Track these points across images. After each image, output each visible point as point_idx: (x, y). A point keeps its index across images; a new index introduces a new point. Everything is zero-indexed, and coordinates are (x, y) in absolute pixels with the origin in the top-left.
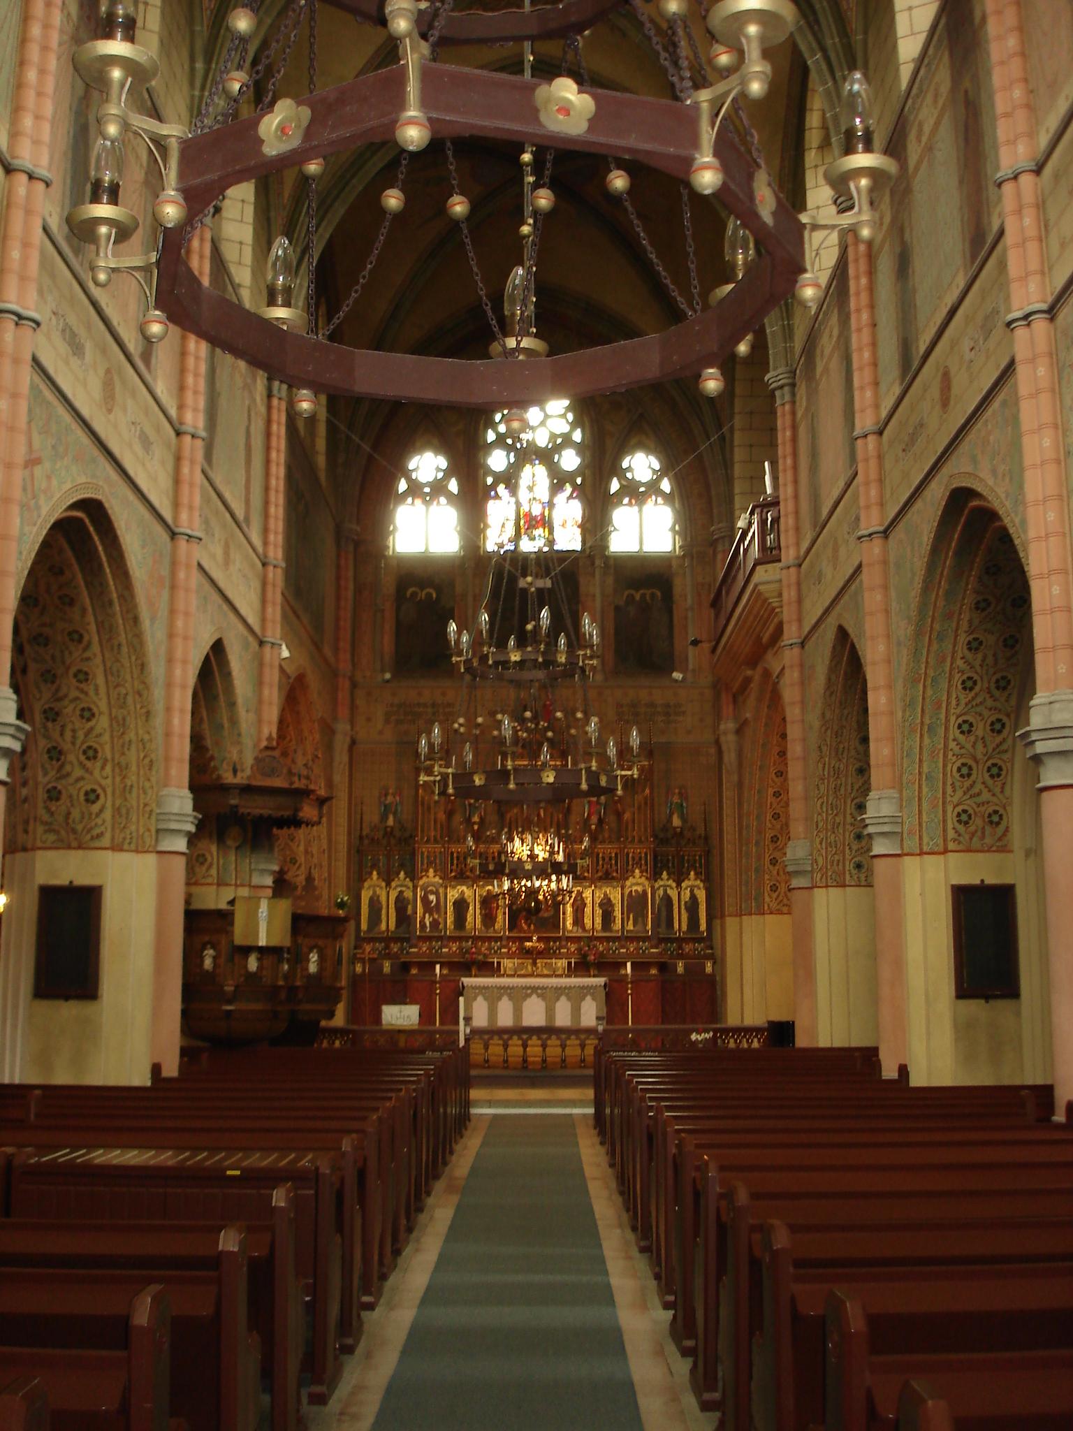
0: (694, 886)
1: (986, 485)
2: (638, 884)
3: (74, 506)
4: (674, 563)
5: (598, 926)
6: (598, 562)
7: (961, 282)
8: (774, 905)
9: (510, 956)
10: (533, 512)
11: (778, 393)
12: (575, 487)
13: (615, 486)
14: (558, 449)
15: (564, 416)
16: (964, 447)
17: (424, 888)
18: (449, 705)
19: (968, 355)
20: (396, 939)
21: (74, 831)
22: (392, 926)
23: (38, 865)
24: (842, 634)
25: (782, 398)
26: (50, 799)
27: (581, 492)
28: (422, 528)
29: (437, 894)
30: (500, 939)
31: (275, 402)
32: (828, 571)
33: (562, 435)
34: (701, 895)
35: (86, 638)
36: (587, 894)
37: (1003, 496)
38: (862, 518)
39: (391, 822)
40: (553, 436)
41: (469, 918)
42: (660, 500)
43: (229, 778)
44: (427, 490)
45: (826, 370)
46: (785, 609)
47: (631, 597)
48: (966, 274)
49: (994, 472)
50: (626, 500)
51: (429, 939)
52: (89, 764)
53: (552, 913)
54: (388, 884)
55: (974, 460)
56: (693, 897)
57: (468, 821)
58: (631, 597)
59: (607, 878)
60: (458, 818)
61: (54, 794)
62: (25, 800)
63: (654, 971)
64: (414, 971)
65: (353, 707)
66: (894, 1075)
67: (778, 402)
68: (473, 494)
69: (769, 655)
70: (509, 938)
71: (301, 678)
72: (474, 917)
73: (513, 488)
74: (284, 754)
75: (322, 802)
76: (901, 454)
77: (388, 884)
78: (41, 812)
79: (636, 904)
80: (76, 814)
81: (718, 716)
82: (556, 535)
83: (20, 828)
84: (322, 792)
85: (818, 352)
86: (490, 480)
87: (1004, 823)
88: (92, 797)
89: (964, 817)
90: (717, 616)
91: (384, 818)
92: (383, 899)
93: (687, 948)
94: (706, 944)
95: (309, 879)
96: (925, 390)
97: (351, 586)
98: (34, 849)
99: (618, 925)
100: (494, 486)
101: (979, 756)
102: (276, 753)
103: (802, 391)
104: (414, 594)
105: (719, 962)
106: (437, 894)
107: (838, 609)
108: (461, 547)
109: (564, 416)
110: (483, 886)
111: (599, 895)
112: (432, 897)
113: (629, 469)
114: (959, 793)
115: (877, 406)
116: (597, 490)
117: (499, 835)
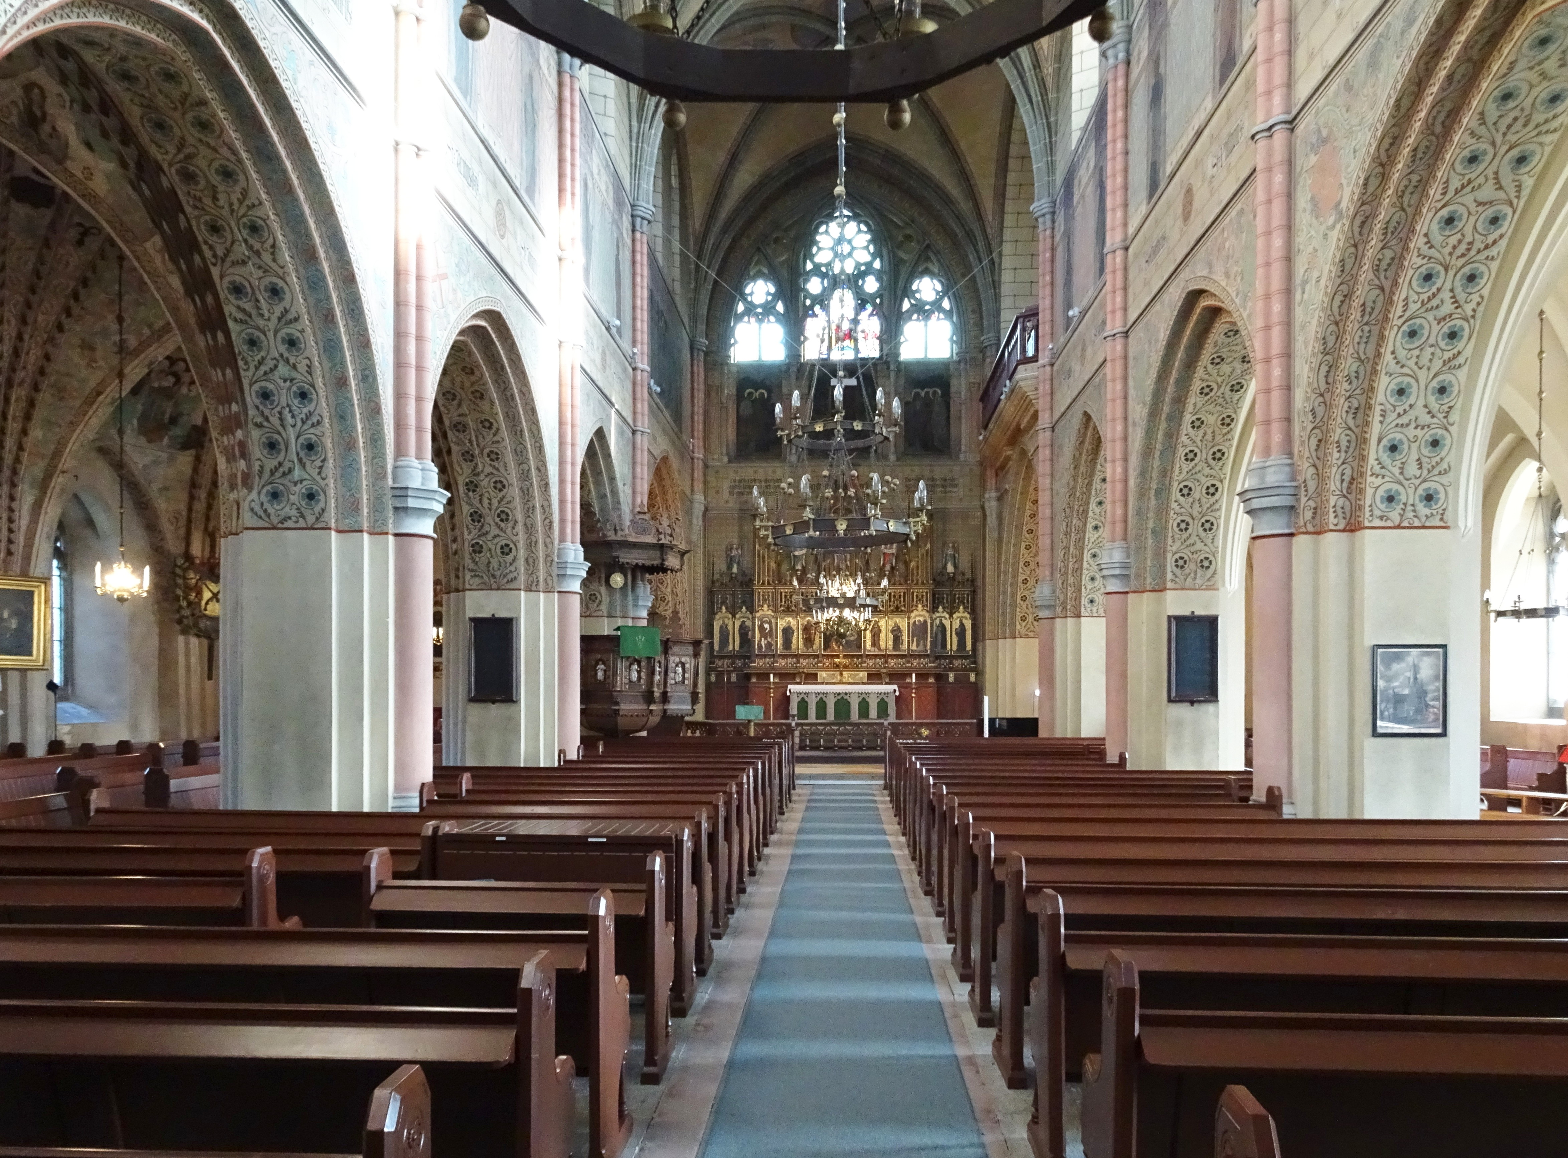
0: (962, 617)
1: (1219, 285)
3: (477, 316)
4: (952, 367)
5: (890, 647)
6: (892, 367)
7: (1209, 104)
8: (1023, 631)
9: (826, 669)
10: (840, 331)
11: (1040, 220)
12: (874, 305)
13: (906, 305)
14: (862, 275)
15: (867, 248)
16: (1202, 252)
17: (761, 619)
19: (1210, 171)
20: (740, 657)
21: (494, 576)
22: (737, 648)
23: (468, 602)
24: (1087, 417)
25: (1044, 224)
26: (474, 551)
27: (879, 311)
28: (756, 342)
29: (770, 623)
30: (817, 656)
31: (638, 235)
32: (1077, 367)
33: (866, 264)
34: (968, 624)
35: (495, 425)
36: (882, 623)
37: (1234, 295)
38: (1109, 322)
39: (735, 569)
40: (858, 265)
41: (794, 641)
42: (942, 316)
43: (611, 536)
44: (759, 310)
45: (1083, 196)
46: (1041, 401)
47: (917, 394)
48: (1214, 97)
49: (1227, 275)
50: (915, 316)
51: (765, 656)
52: (502, 525)
54: (734, 616)
55: (1210, 266)
56: (962, 625)
57: (793, 570)
58: (917, 394)
59: (897, 610)
60: (785, 567)
61: (477, 548)
62: (456, 553)
63: (931, 680)
64: (754, 680)
65: (705, 483)
66: (1116, 760)
67: (1041, 227)
68: (795, 311)
69: (1026, 438)
71: (665, 459)
72: (798, 641)
73: (825, 308)
74: (654, 518)
75: (682, 554)
76: (1144, 265)
77: (734, 616)
78: (468, 562)
79: (919, 631)
80: (494, 563)
81: (983, 487)
82: (860, 346)
83: (453, 576)
84: (683, 547)
85: (1076, 182)
86: (808, 302)
87: (1212, 567)
88: (506, 550)
89: (1181, 563)
90: (984, 408)
91: (730, 567)
92: (730, 627)
93: (957, 663)
94: (973, 660)
95: (675, 613)
96: (1169, 208)
97: (702, 387)
98: (464, 590)
99: (905, 646)
100: (811, 307)
101: (1195, 514)
102: (647, 517)
103: (1060, 218)
104: (750, 394)
105: (979, 673)
106: (770, 623)
107: (1083, 397)
108: (787, 356)
109: (867, 248)
111: (891, 624)
112: (766, 626)
113: (918, 291)
114: (1178, 544)
115: (1125, 225)
116: (892, 310)
117: (818, 577)
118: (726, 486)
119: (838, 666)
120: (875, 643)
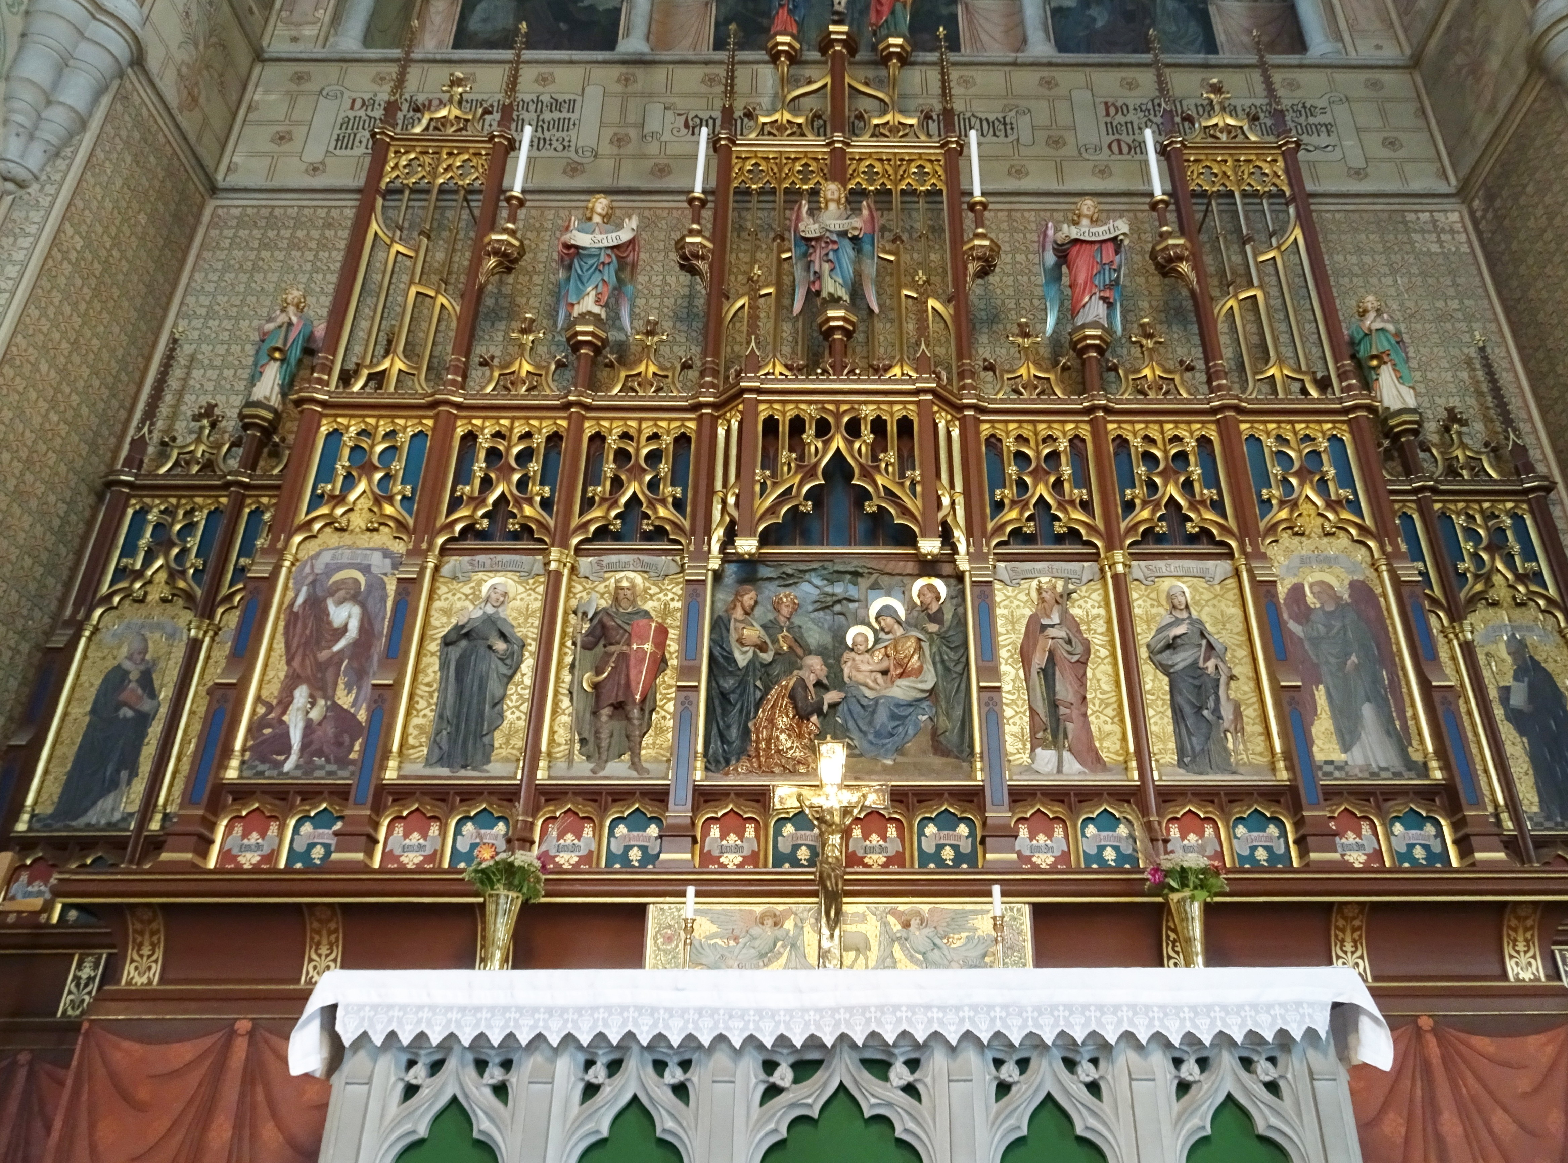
2: (1327, 562)
18: (556, 105)
41: (515, 713)
70: (704, 797)
118: (326, 119)
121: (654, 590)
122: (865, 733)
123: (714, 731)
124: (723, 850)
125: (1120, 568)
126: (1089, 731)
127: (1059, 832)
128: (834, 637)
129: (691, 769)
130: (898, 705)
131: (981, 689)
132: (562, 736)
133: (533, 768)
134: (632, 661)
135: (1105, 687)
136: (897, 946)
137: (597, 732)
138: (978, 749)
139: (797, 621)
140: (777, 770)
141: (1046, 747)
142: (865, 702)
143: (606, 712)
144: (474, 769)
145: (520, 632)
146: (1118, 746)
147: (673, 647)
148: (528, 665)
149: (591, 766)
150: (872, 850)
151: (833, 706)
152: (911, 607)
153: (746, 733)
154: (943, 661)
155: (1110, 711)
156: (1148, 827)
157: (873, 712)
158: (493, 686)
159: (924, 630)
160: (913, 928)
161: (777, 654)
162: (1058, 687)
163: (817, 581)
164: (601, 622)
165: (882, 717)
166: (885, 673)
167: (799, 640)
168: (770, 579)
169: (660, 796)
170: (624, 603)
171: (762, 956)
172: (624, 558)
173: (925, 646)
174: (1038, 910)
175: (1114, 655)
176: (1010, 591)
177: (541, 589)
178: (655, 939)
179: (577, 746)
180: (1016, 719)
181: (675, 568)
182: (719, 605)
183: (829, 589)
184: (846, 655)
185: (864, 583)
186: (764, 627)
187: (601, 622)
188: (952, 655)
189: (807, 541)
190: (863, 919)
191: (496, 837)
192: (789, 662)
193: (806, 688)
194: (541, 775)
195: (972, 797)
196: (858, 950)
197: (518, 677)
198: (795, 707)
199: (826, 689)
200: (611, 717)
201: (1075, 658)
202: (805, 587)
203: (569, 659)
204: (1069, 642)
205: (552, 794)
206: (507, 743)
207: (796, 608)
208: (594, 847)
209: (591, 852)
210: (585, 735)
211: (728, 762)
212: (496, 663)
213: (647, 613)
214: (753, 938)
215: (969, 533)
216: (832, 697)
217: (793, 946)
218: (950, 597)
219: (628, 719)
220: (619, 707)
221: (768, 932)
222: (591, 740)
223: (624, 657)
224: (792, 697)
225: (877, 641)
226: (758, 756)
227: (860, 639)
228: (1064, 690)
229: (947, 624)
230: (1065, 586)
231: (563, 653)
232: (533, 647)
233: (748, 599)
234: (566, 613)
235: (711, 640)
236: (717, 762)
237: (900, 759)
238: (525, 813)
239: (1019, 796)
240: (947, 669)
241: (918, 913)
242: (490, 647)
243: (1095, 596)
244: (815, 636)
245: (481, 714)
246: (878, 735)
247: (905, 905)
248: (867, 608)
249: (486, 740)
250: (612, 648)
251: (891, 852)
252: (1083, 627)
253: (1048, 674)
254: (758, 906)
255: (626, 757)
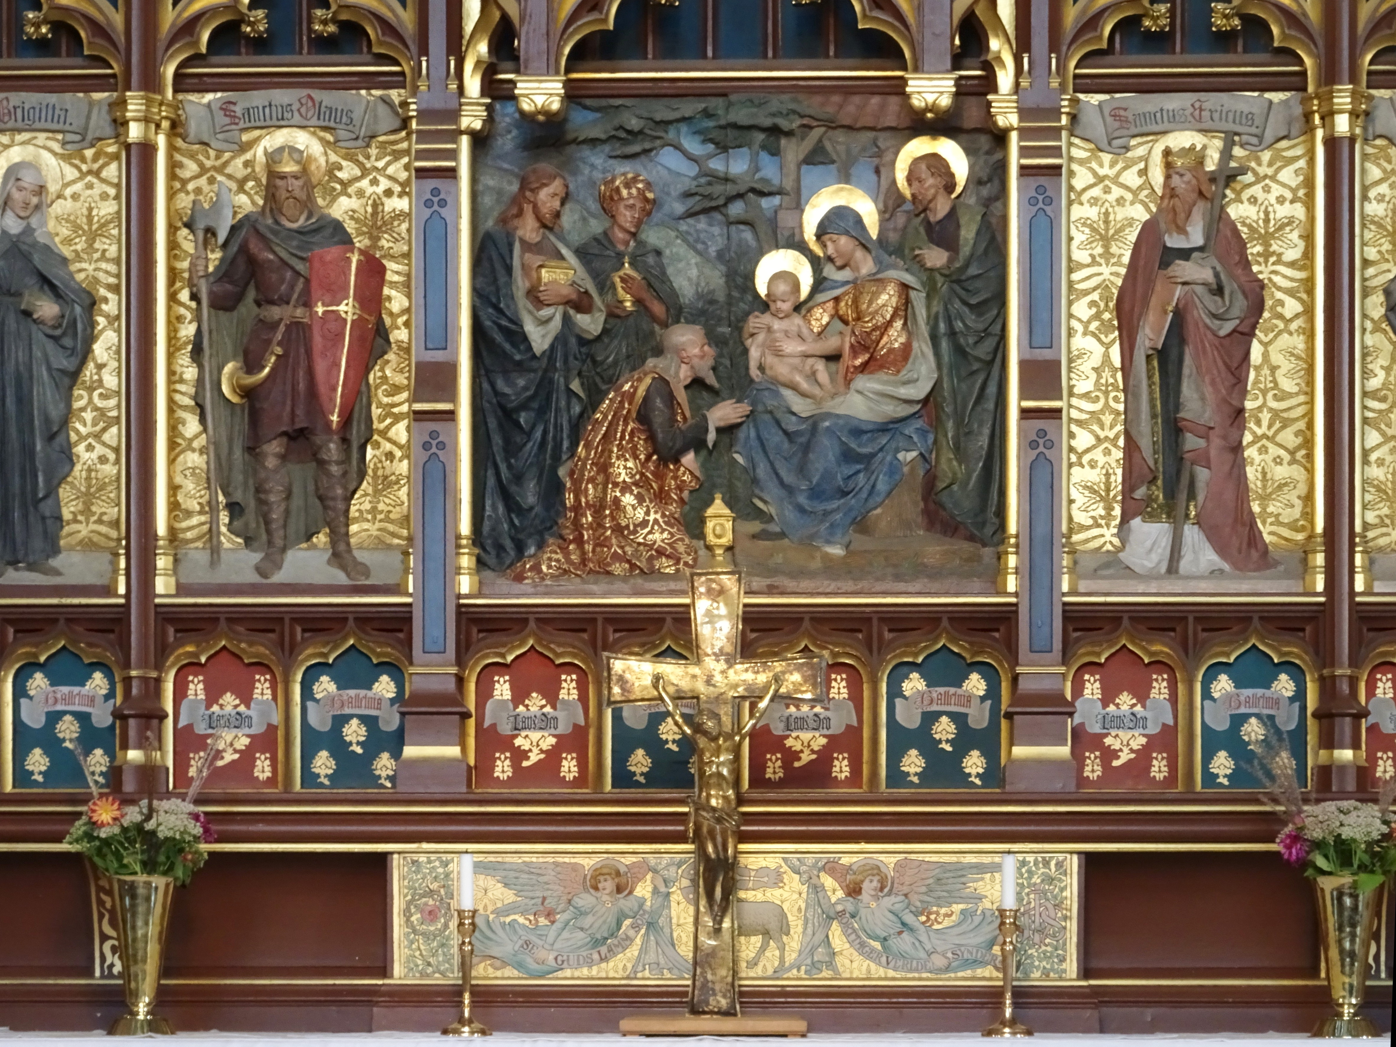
36: (1275, 201)
41: (95, 451)
53: (921, 376)
70: (478, 627)
110: (237, 125)
119: (675, 770)
120: (1174, 468)
121: (348, 171)
122: (790, 490)
123: (491, 482)
124: (520, 725)
125: (1342, 124)
126: (1242, 477)
127: (1160, 689)
128: (730, 276)
129: (449, 572)
130: (857, 431)
131: (1025, 413)
132: (193, 495)
133: (147, 572)
134: (318, 341)
135: (1288, 385)
136: (835, 925)
137: (267, 523)
138: (1012, 528)
139: (652, 237)
140: (618, 568)
141: (1151, 517)
142: (792, 425)
143: (273, 448)
144: (31, 567)
145: (83, 271)
146: (1297, 512)
147: (396, 301)
148: (107, 344)
149: (256, 557)
150: (801, 723)
151: (728, 431)
152: (891, 203)
153: (554, 489)
154: (952, 334)
155: (1289, 437)
156: (1327, 687)
157: (806, 449)
158: (44, 393)
159: (917, 263)
160: (865, 896)
161: (611, 315)
162: (1188, 391)
163: (693, 145)
164: (244, 249)
165: (825, 457)
166: (833, 358)
167: (655, 282)
168: (593, 142)
169: (396, 624)
170: (289, 207)
171: (597, 943)
172: (281, 96)
173: (918, 299)
174: (1090, 860)
175: (1309, 311)
176: (1106, 164)
177: (112, 171)
178: (407, 914)
179: (224, 518)
180: (1097, 455)
181: (387, 120)
182: (487, 200)
183: (717, 165)
184: (756, 321)
185: (793, 151)
186: (582, 253)
187: (244, 249)
188: (971, 319)
189: (671, 52)
190: (777, 879)
191: (92, 700)
192: (639, 335)
193: (670, 398)
194: (163, 585)
195: (993, 628)
196: (766, 934)
197: (89, 371)
198: (651, 438)
199: (716, 395)
200: (283, 458)
201: (1228, 327)
202: (669, 159)
203: (188, 331)
204: (1219, 291)
205: (186, 623)
206: (87, 511)
207: (649, 207)
208: (276, 718)
209: (272, 729)
210: (238, 496)
211: (520, 548)
212: (43, 348)
213: (338, 226)
214: (581, 913)
215: (1023, 44)
216: (724, 413)
217: (651, 925)
218: (975, 181)
219: (321, 464)
220: (301, 439)
221: (604, 903)
222: (251, 504)
223: (299, 333)
224: (643, 417)
225: (819, 284)
226: (579, 541)
227: (782, 288)
228: (1196, 401)
229: (965, 251)
230: (1226, 154)
231: (175, 319)
232: (112, 305)
233: (547, 197)
234: (172, 229)
235: (476, 291)
236: (500, 548)
237: (860, 542)
238: (144, 664)
239: (1085, 623)
240: (960, 351)
241: (876, 870)
242: (27, 314)
243: (1287, 175)
244: (690, 274)
245: (28, 452)
246: (816, 494)
247: (851, 854)
248: (799, 208)
249: (46, 508)
250: (275, 312)
251: (837, 728)
252: (1254, 249)
253: (1168, 360)
254: (587, 857)
255: (321, 539)
